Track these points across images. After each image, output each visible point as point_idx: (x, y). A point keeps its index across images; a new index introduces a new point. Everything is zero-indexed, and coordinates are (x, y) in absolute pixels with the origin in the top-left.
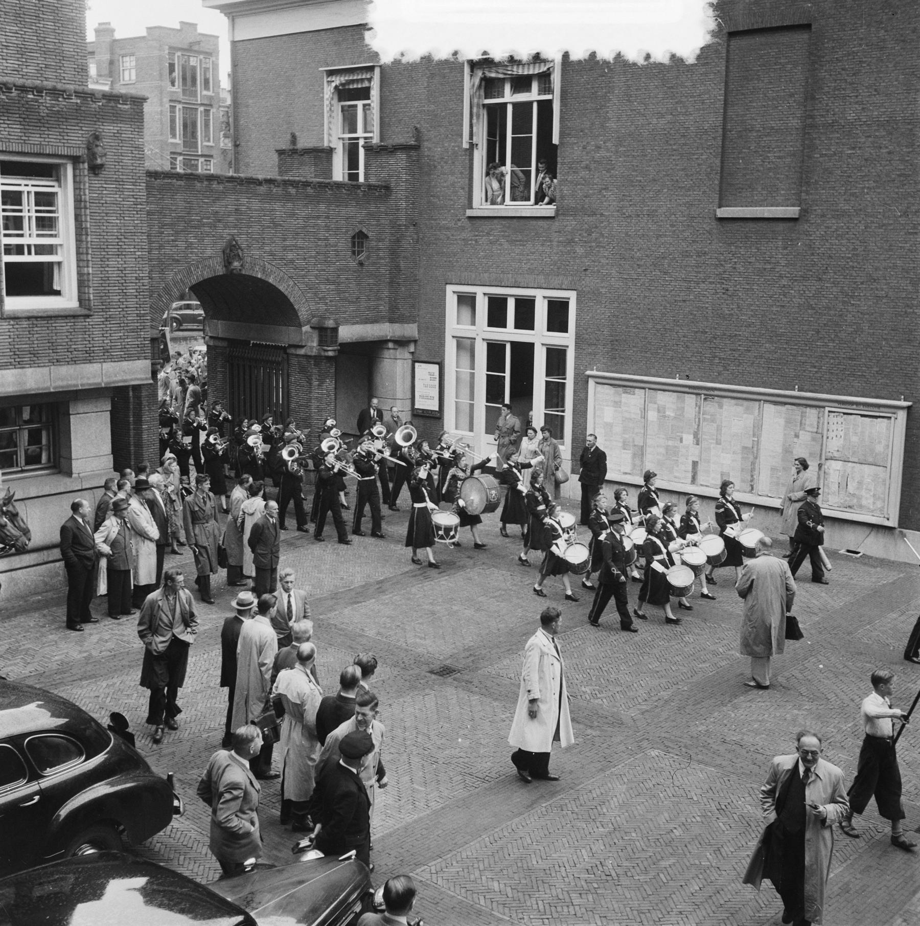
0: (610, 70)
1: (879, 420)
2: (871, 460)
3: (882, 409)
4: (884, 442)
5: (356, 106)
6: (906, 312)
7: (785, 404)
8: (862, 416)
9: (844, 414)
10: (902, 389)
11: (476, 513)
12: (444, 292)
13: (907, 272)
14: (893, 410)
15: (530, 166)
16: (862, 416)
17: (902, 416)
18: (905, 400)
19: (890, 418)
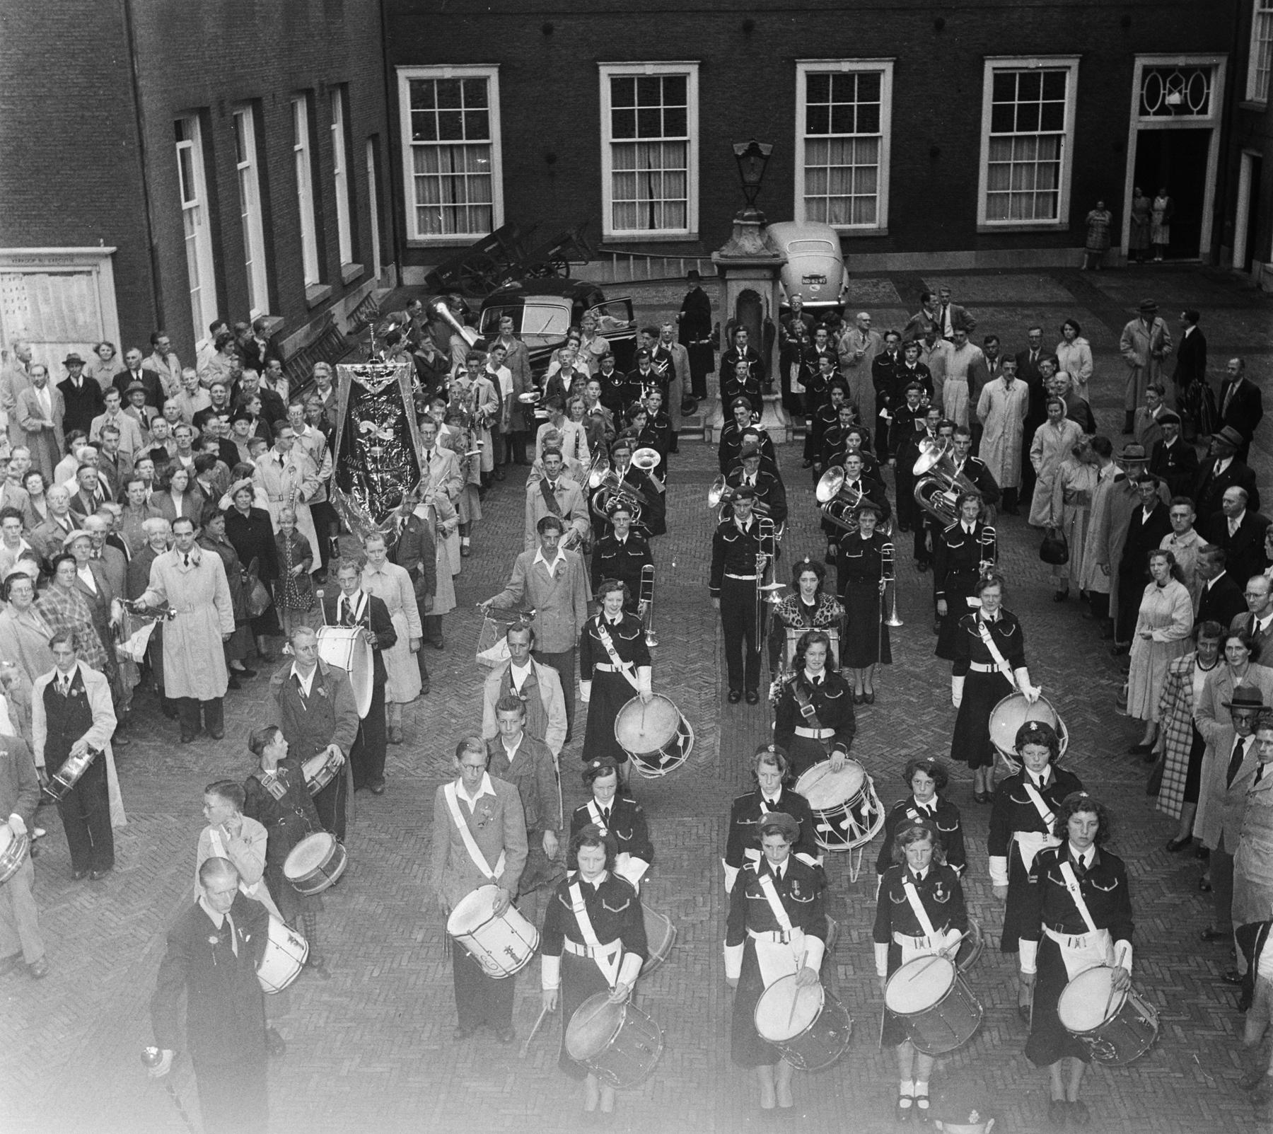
0: (988, 340)
1: (76, 277)
2: (74, 336)
3: (77, 261)
4: (89, 309)
5: (1141, 133)
6: (83, 117)
7: (34, 273)
8: (51, 274)
9: (25, 274)
10: (99, 229)
11: (627, 747)
12: (597, 73)
13: (73, 57)
14: (95, 261)
15: (833, 132)
16: (51, 274)
17: (107, 268)
18: (106, 245)
19: (89, 273)
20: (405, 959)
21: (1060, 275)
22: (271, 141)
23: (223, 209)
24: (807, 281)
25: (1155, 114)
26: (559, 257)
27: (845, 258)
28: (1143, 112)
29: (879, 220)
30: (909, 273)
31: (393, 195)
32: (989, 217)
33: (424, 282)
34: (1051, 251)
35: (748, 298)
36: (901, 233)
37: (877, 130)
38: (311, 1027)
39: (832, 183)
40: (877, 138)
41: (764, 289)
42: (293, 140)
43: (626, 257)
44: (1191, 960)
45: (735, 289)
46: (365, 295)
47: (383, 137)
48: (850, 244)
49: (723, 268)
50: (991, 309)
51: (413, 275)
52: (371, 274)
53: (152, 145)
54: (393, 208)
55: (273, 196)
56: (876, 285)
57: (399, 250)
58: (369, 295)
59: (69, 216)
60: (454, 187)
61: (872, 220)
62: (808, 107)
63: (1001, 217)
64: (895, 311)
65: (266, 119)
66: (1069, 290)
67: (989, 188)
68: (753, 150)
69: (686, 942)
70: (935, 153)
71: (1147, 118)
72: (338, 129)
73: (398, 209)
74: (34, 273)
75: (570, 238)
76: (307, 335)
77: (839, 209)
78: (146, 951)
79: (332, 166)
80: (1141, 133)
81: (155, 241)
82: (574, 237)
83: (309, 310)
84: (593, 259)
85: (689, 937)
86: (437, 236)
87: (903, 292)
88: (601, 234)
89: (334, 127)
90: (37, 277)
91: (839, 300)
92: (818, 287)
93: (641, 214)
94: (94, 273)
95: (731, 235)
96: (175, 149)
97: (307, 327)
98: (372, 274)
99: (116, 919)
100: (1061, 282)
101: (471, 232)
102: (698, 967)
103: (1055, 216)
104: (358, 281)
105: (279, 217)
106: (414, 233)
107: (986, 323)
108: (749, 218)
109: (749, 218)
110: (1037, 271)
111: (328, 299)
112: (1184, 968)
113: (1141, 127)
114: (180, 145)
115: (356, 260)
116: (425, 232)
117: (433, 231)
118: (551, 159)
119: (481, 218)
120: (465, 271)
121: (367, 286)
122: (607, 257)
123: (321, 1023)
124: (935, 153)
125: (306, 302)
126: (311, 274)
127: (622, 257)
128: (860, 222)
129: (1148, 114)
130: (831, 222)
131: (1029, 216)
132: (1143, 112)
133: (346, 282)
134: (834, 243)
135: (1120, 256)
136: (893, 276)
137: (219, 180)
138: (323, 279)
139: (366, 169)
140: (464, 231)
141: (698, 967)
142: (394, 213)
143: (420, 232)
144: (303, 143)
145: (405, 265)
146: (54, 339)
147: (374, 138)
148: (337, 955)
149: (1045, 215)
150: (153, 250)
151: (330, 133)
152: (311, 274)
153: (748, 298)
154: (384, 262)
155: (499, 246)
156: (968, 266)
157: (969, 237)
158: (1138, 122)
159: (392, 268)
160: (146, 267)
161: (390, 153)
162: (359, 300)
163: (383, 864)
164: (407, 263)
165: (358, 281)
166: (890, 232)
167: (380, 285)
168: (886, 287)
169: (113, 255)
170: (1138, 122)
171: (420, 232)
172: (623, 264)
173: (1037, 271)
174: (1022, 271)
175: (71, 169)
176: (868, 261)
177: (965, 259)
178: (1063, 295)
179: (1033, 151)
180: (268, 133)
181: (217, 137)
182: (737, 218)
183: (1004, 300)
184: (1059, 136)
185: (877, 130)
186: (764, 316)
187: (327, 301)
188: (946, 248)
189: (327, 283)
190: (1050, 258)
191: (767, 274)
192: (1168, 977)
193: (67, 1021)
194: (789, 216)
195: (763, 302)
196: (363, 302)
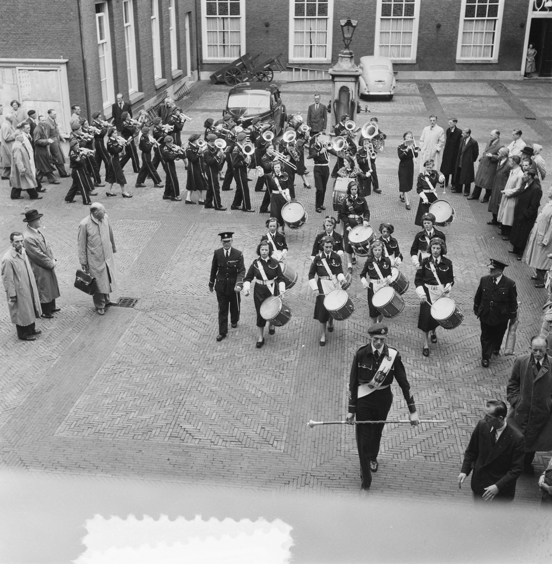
2: (50, 98)
3: (51, 65)
5: (533, 20)
7: (33, 70)
8: (40, 70)
9: (29, 70)
16: (40, 70)
17: (64, 68)
20: (163, 371)
21: (493, 83)
22: (140, 13)
23: (117, 44)
24: (377, 83)
25: (540, 10)
26: (269, 69)
27: (395, 73)
28: (534, 9)
29: (411, 57)
30: (425, 80)
31: (197, 39)
32: (462, 56)
33: (210, 79)
34: (489, 72)
35: (344, 90)
36: (421, 63)
37: (496, 16)
38: (120, 398)
39: (392, 38)
40: (412, 19)
41: (351, 86)
42: (151, 13)
43: (299, 70)
44: (501, 387)
45: (339, 85)
46: (183, 84)
47: (193, 14)
48: (397, 67)
49: (334, 76)
50: (459, 98)
51: (205, 76)
52: (185, 74)
53: (84, 15)
54: (197, 45)
55: (141, 38)
56: (409, 86)
57: (199, 64)
58: (184, 85)
59: (48, 45)
60: (224, 37)
61: (409, 56)
62: (296, 4)
63: (468, 56)
64: (416, 97)
65: (138, 4)
66: (496, 90)
67: (463, 43)
68: (349, 23)
69: (283, 369)
70: (439, 26)
71: (535, 12)
72: (172, 9)
73: (199, 46)
74: (33, 70)
75: (274, 61)
76: (155, 101)
77: (395, 50)
78: (55, 363)
79: (169, 26)
80: (533, 20)
81: (85, 57)
82: (276, 60)
83: (156, 90)
84: (284, 70)
85: (285, 368)
86: (216, 58)
87: (420, 89)
88: (455, 59)
89: (170, 8)
90: (34, 71)
91: (390, 92)
92: (381, 86)
93: (220, 50)
94: (58, 71)
95: (337, 60)
96: (95, 17)
97: (155, 97)
98: (186, 75)
99: (44, 349)
100: (492, 86)
101: (231, 57)
102: (287, 380)
103: (492, 56)
104: (180, 77)
105: (144, 48)
106: (206, 57)
107: (456, 104)
108: (346, 54)
109: (346, 54)
110: (482, 81)
111: (165, 85)
112: (498, 391)
113: (534, 17)
114: (98, 15)
115: (179, 68)
116: (211, 56)
117: (214, 56)
118: (267, 25)
119: (236, 50)
120: (227, 74)
121: (184, 80)
122: (290, 69)
123: (124, 396)
124: (439, 26)
125: (155, 87)
126: (158, 74)
127: (297, 70)
128: (404, 56)
129: (536, 10)
130: (390, 56)
131: (480, 56)
132: (534, 9)
133: (174, 78)
134: (390, 67)
135: (520, 75)
136: (418, 82)
137: (115, 31)
138: (164, 77)
139: (185, 27)
140: (228, 56)
141: (287, 380)
142: (197, 48)
143: (209, 56)
144: (156, 14)
145: (201, 71)
146: (41, 99)
147: (189, 13)
148: (134, 369)
149: (487, 55)
150: (84, 62)
151: (169, 11)
152: (158, 74)
153: (344, 90)
154: (192, 69)
155: (243, 63)
156: (450, 78)
157: (452, 65)
158: (532, 15)
159: (196, 72)
160: (80, 69)
161: (196, 20)
162: (180, 86)
163: (159, 330)
164: (203, 70)
165: (180, 77)
166: (417, 62)
167: (190, 79)
168: (414, 87)
169: (67, 63)
170: (532, 15)
171: (209, 56)
172: (298, 73)
173: (482, 81)
174: (475, 81)
175: (49, 24)
176: (404, 75)
177: (450, 75)
178: (493, 92)
179: (483, 26)
180: (139, 10)
181: (115, 11)
182: (341, 53)
183: (465, 94)
184: (495, 20)
185: (496, 16)
186: (351, 98)
187: (164, 86)
188: (441, 69)
189: (165, 78)
190: (488, 75)
191: (353, 79)
192: (490, 395)
193: (18, 391)
194: (372, 54)
195: (350, 92)
196: (182, 87)
